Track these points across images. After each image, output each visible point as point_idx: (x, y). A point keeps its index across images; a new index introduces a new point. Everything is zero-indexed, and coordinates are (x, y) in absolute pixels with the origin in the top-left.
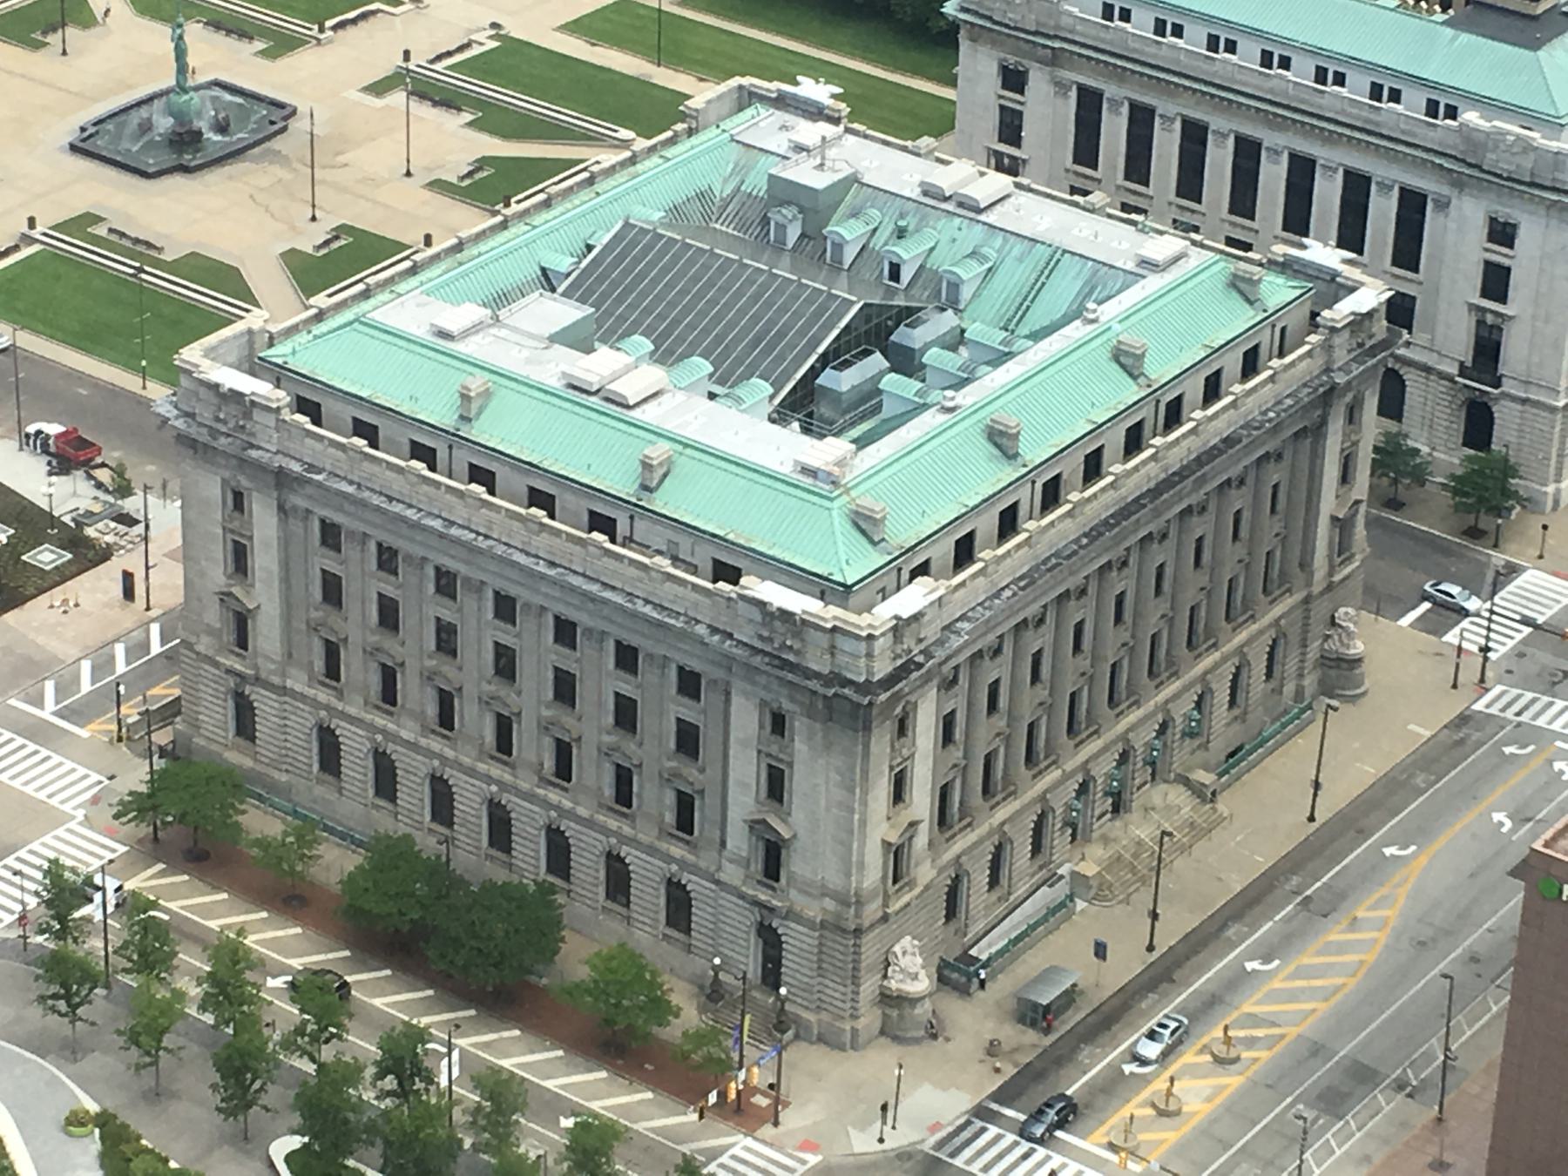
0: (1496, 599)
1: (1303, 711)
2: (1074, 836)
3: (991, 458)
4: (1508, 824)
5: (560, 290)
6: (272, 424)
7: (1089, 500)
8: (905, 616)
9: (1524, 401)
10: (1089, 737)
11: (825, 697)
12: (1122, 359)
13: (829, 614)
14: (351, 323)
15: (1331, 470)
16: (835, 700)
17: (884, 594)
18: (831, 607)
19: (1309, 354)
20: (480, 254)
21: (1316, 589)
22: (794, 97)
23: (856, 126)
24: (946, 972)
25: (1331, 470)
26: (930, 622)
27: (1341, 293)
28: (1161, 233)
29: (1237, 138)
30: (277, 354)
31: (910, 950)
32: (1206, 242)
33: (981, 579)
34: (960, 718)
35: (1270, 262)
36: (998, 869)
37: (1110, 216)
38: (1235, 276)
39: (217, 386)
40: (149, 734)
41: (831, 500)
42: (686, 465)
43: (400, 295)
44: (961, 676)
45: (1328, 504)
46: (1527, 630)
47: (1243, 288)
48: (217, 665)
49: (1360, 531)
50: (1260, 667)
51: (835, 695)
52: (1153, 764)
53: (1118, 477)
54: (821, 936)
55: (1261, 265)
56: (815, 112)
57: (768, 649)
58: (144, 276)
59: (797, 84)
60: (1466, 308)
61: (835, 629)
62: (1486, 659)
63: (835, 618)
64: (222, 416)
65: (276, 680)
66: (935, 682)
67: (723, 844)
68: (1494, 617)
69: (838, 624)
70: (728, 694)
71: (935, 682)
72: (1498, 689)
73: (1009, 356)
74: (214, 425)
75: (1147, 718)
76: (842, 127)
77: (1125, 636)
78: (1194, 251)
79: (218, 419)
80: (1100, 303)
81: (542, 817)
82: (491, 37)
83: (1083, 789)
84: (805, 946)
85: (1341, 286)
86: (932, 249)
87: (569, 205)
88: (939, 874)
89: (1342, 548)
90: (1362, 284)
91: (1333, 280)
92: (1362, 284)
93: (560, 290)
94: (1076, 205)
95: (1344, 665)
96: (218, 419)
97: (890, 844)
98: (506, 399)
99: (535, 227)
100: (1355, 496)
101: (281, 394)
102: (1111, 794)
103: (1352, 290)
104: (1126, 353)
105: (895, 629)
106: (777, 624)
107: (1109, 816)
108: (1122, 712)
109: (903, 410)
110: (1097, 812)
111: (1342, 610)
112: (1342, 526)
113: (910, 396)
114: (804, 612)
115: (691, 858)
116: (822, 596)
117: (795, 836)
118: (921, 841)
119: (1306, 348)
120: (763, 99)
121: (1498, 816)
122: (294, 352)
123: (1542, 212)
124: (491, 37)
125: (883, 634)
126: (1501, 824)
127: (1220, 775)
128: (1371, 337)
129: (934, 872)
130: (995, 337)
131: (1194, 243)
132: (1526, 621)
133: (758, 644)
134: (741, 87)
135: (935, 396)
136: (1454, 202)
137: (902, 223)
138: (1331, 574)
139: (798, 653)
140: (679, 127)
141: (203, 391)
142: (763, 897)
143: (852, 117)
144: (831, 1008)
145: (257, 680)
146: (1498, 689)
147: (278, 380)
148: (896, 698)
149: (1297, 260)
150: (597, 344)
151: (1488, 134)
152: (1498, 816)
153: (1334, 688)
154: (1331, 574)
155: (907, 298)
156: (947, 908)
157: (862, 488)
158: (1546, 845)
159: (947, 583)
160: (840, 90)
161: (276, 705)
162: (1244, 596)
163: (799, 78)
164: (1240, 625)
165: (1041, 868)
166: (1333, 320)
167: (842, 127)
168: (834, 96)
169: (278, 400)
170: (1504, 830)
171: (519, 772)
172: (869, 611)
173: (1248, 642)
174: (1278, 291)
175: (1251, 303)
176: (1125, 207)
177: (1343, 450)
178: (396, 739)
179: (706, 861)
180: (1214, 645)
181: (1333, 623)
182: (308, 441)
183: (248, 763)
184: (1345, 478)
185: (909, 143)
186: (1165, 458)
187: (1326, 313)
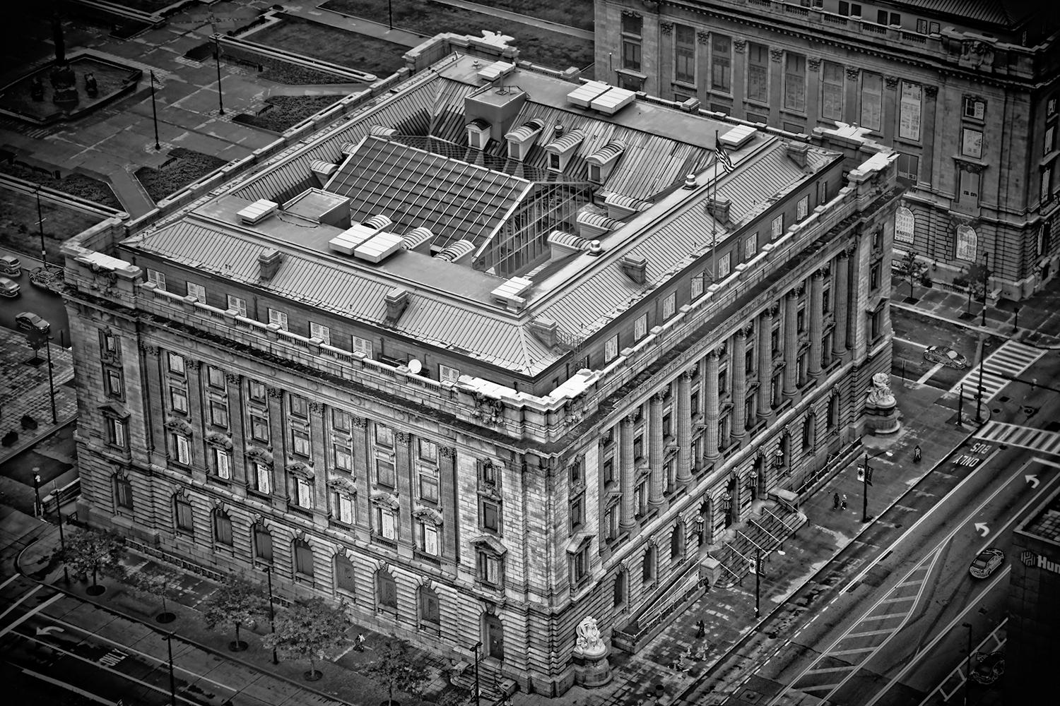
0: (984, 362)
1: (854, 446)
2: (700, 541)
3: (627, 285)
4: (987, 530)
5: (326, 187)
6: (130, 289)
7: (696, 310)
8: (572, 396)
9: (998, 225)
10: (733, 450)
11: (521, 455)
12: (792, 155)
13: (523, 397)
14: (181, 218)
15: (863, 280)
16: (527, 456)
17: (558, 382)
18: (521, 393)
19: (843, 201)
20: (269, 165)
21: (858, 362)
22: (481, 45)
23: (523, 62)
24: (617, 640)
25: (863, 280)
26: (590, 400)
27: (864, 157)
28: (738, 123)
29: (787, 55)
30: (133, 241)
31: (590, 625)
32: (768, 128)
33: (625, 368)
34: (781, 332)
35: (813, 139)
36: (649, 568)
37: (702, 114)
38: (789, 150)
39: (91, 265)
40: (59, 508)
41: (519, 319)
42: (418, 301)
43: (216, 196)
44: (644, 413)
45: (863, 304)
46: (1007, 382)
47: (795, 158)
48: (104, 458)
49: (887, 321)
50: (822, 418)
51: (528, 453)
52: (752, 489)
53: (743, 272)
54: (529, 620)
55: (807, 142)
56: (495, 55)
57: (480, 424)
58: (40, 192)
59: (482, 36)
60: (953, 163)
61: (524, 408)
62: (980, 403)
63: (524, 400)
64: (95, 286)
65: (145, 465)
66: (597, 441)
67: (458, 560)
68: (984, 375)
69: (526, 404)
70: (454, 458)
71: (597, 441)
72: (992, 423)
73: (636, 214)
74: (91, 293)
75: (746, 457)
76: (514, 64)
77: (829, 321)
78: (760, 134)
79: (94, 289)
80: (697, 174)
81: (332, 548)
82: (273, 16)
83: (705, 509)
84: (518, 628)
85: (863, 153)
86: (580, 144)
87: (415, 79)
88: (608, 572)
89: (874, 335)
90: (878, 150)
91: (857, 149)
92: (878, 150)
93: (326, 187)
94: (677, 107)
95: (882, 413)
96: (94, 289)
97: (572, 554)
98: (294, 264)
99: (306, 144)
100: (882, 296)
101: (136, 269)
102: (726, 511)
103: (871, 155)
104: (795, 152)
105: (565, 407)
106: (485, 407)
107: (724, 526)
108: (729, 454)
109: (566, 255)
110: (716, 523)
111: (878, 375)
112: (874, 317)
113: (627, 207)
114: (503, 397)
115: (436, 570)
116: (515, 387)
117: (506, 552)
118: (594, 550)
119: (737, 274)
120: (459, 47)
121: (979, 526)
122: (144, 239)
123: (1002, 93)
124: (273, 16)
125: (558, 411)
126: (982, 531)
127: (800, 493)
128: (885, 187)
129: (604, 572)
130: (626, 203)
131: (759, 129)
132: (1005, 376)
133: (473, 422)
134: (443, 41)
135: (586, 245)
136: (941, 90)
137: (558, 127)
138: (868, 351)
139: (501, 425)
140: (403, 70)
141: (82, 270)
142: (486, 595)
143: (521, 57)
144: (539, 669)
145: (132, 467)
146: (992, 423)
147: (134, 259)
148: (568, 454)
149: (832, 137)
150: (353, 223)
151: (961, 41)
152: (979, 526)
153: (874, 429)
154: (868, 351)
155: (565, 179)
156: (615, 596)
157: (538, 311)
158: (1025, 529)
159: (601, 372)
160: (511, 39)
161: (145, 483)
162: (809, 369)
163: (484, 32)
164: (807, 390)
165: (679, 564)
166: (857, 176)
167: (514, 64)
168: (508, 43)
169: (134, 273)
170: (984, 535)
171: (315, 519)
172: (548, 395)
173: (787, 422)
174: (819, 158)
175: (802, 168)
176: (714, 108)
177: (871, 266)
178: (229, 500)
179: (446, 570)
180: (790, 404)
181: (871, 384)
182: (157, 300)
183: (129, 524)
184: (874, 286)
185: (561, 72)
186: (773, 258)
187: (853, 172)
